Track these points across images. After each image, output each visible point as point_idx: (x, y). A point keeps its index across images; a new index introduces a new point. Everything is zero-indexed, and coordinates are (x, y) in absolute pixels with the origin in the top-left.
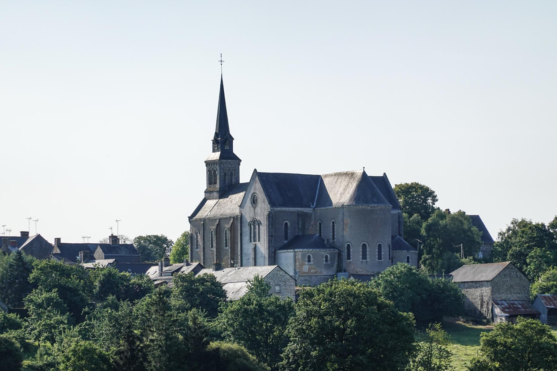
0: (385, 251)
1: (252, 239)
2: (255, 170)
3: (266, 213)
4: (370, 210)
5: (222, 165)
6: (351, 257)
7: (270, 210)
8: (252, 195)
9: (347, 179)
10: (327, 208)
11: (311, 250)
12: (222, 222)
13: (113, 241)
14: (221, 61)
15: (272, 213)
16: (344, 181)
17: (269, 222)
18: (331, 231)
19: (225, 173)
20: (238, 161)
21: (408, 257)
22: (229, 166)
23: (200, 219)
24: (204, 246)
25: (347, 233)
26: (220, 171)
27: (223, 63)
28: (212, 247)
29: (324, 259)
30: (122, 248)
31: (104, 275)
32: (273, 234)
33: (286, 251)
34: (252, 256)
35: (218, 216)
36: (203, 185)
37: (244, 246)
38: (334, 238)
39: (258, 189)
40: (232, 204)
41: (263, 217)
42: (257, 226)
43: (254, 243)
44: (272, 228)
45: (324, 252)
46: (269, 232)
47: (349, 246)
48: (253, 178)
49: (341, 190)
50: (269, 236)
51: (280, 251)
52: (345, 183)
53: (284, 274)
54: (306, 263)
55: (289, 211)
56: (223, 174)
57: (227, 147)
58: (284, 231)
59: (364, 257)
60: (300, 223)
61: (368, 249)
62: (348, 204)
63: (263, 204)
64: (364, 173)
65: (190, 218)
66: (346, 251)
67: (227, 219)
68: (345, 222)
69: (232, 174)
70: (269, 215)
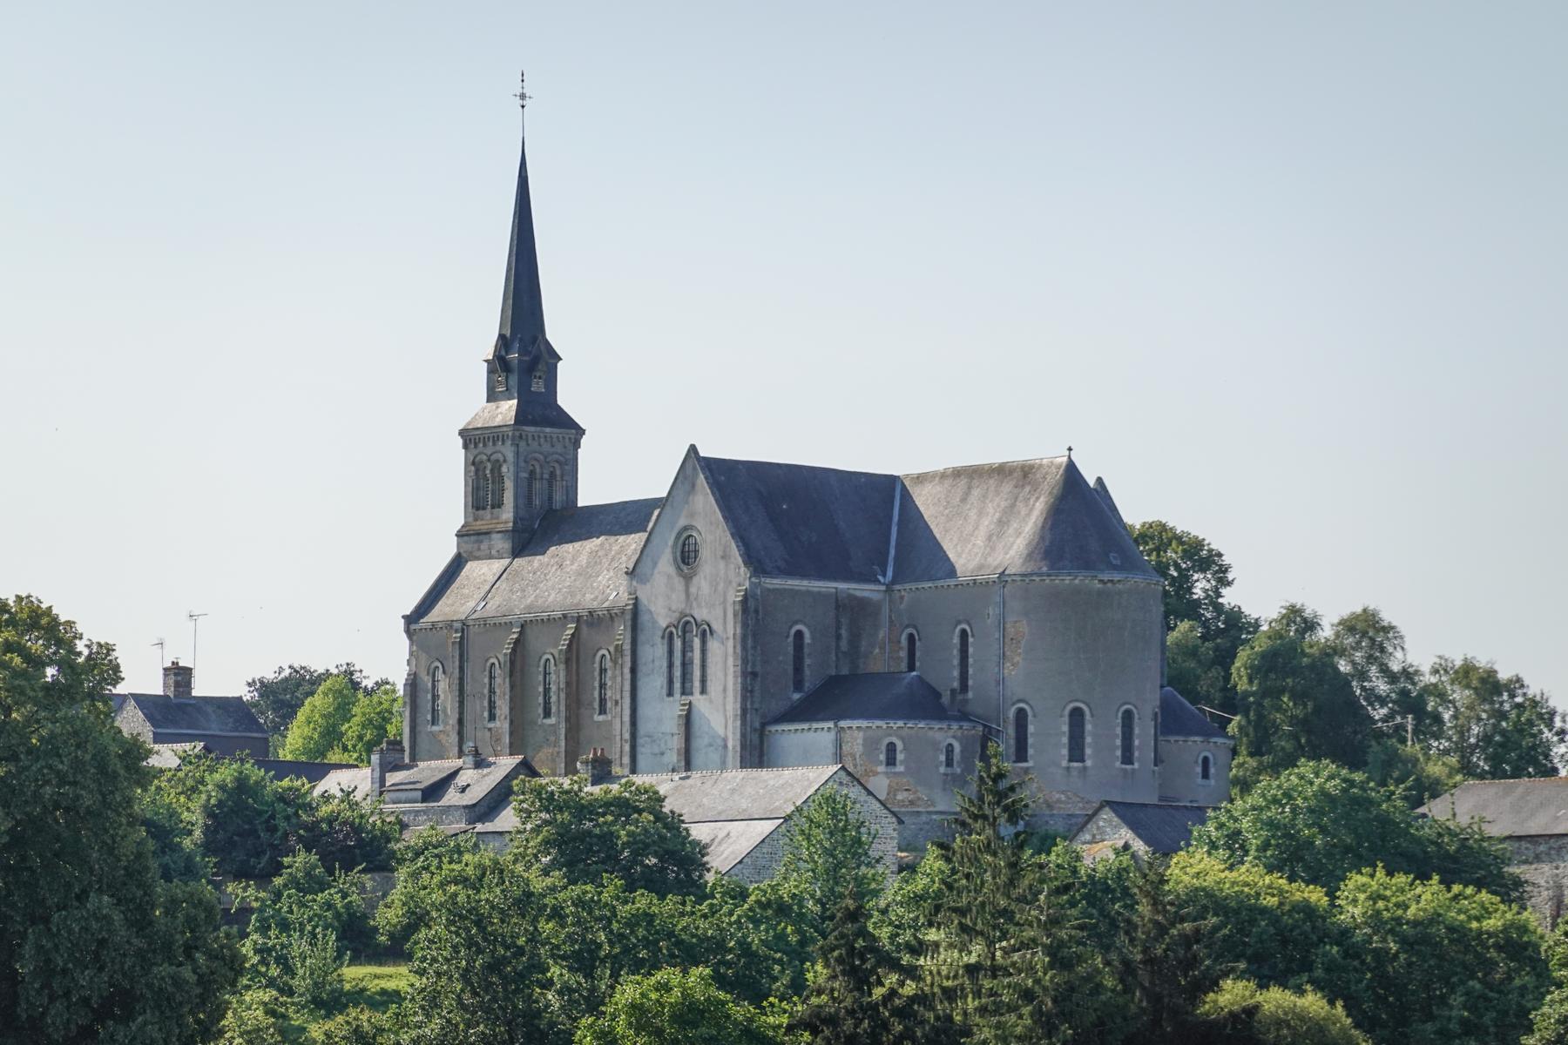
0: (1144, 732)
1: (677, 685)
2: (693, 449)
4: (1100, 593)
5: (523, 444)
6: (1031, 751)
7: (747, 584)
8: (679, 534)
10: (940, 583)
11: (900, 723)
12: (528, 631)
13: (177, 684)
14: (523, 96)
15: (754, 596)
16: (991, 504)
17: (745, 625)
18: (956, 662)
19: (532, 473)
20: (575, 432)
21: (1206, 760)
22: (546, 447)
23: (449, 625)
24: (461, 713)
25: (1018, 669)
26: (517, 464)
27: (527, 102)
28: (492, 717)
29: (943, 758)
30: (210, 709)
31: (221, 787)
32: (758, 669)
33: (806, 726)
34: (677, 743)
36: (453, 510)
37: (645, 711)
38: (964, 686)
40: (581, 575)
41: (719, 611)
42: (697, 642)
43: (686, 700)
44: (754, 648)
45: (944, 734)
46: (745, 661)
47: (1021, 714)
48: (683, 477)
49: (987, 523)
50: (744, 674)
51: (780, 728)
52: (994, 509)
53: (863, 797)
54: (881, 769)
55: (809, 593)
56: (525, 476)
57: (538, 386)
58: (790, 658)
59: (1076, 753)
60: (844, 632)
61: (1088, 727)
62: (1023, 570)
63: (722, 564)
65: (410, 620)
66: (1011, 731)
67: (554, 623)
68: (1011, 630)
69: (552, 474)
70: (745, 601)
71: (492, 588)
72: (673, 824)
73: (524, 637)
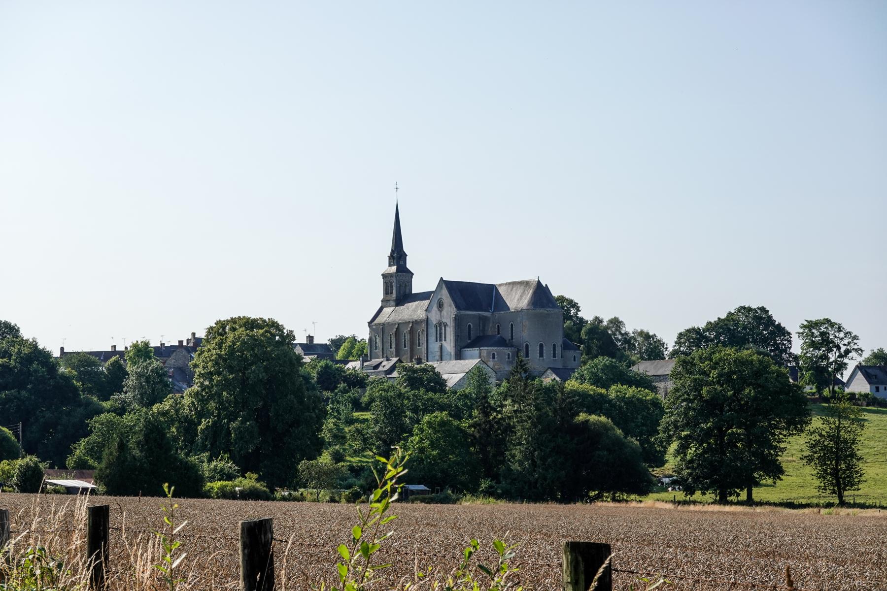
0: (559, 350)
3: (453, 316)
9: (522, 287)
16: (519, 291)
23: (379, 324)
25: (525, 334)
31: (321, 367)
34: (439, 354)
35: (397, 321)
37: (430, 346)
39: (445, 294)
40: (414, 311)
45: (508, 351)
47: (527, 345)
49: (517, 297)
52: (519, 292)
56: (398, 286)
57: (402, 263)
59: (541, 355)
64: (539, 281)
65: (370, 323)
71: (390, 314)
72: (438, 375)
73: (400, 326)
